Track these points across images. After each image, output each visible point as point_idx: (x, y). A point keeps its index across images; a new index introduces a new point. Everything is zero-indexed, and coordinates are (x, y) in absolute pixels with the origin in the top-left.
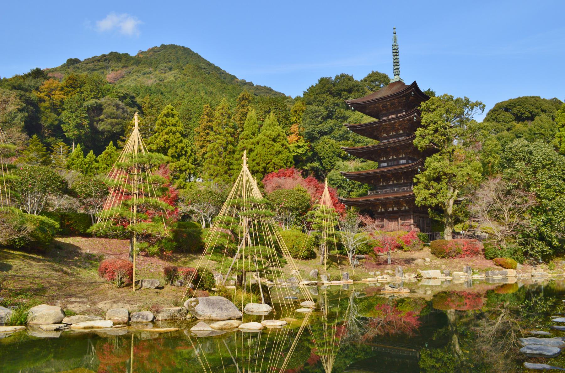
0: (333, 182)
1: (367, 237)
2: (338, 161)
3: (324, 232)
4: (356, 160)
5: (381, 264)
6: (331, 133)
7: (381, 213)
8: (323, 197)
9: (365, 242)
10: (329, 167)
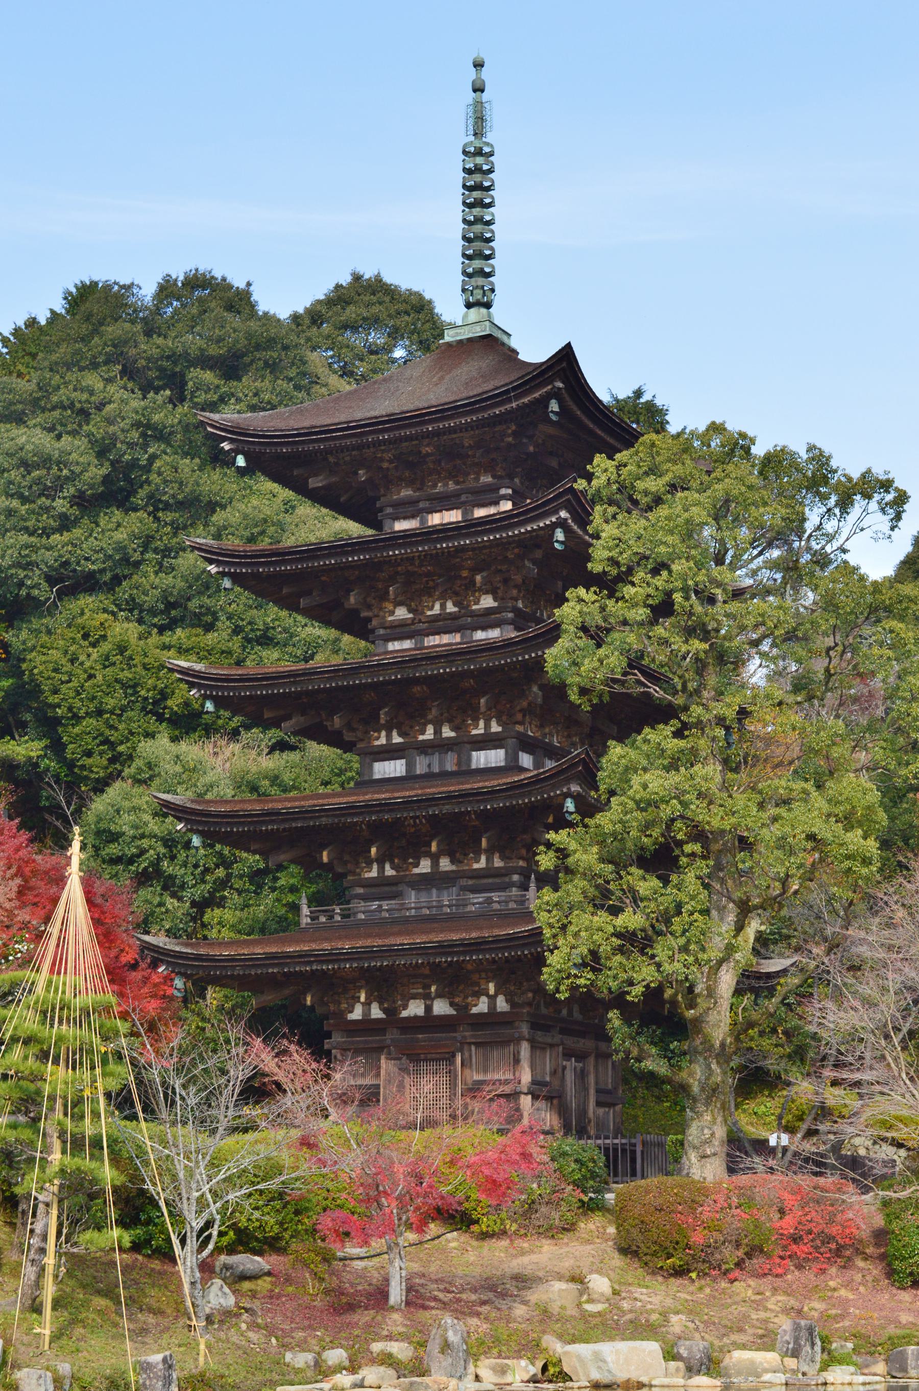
0: (113, 849)
1: (285, 1158)
2: (150, 735)
3: (49, 1126)
4: (245, 736)
5: (351, 1307)
6: (117, 580)
7: (367, 1026)
8: (54, 930)
9: (273, 1185)
10: (98, 764)
